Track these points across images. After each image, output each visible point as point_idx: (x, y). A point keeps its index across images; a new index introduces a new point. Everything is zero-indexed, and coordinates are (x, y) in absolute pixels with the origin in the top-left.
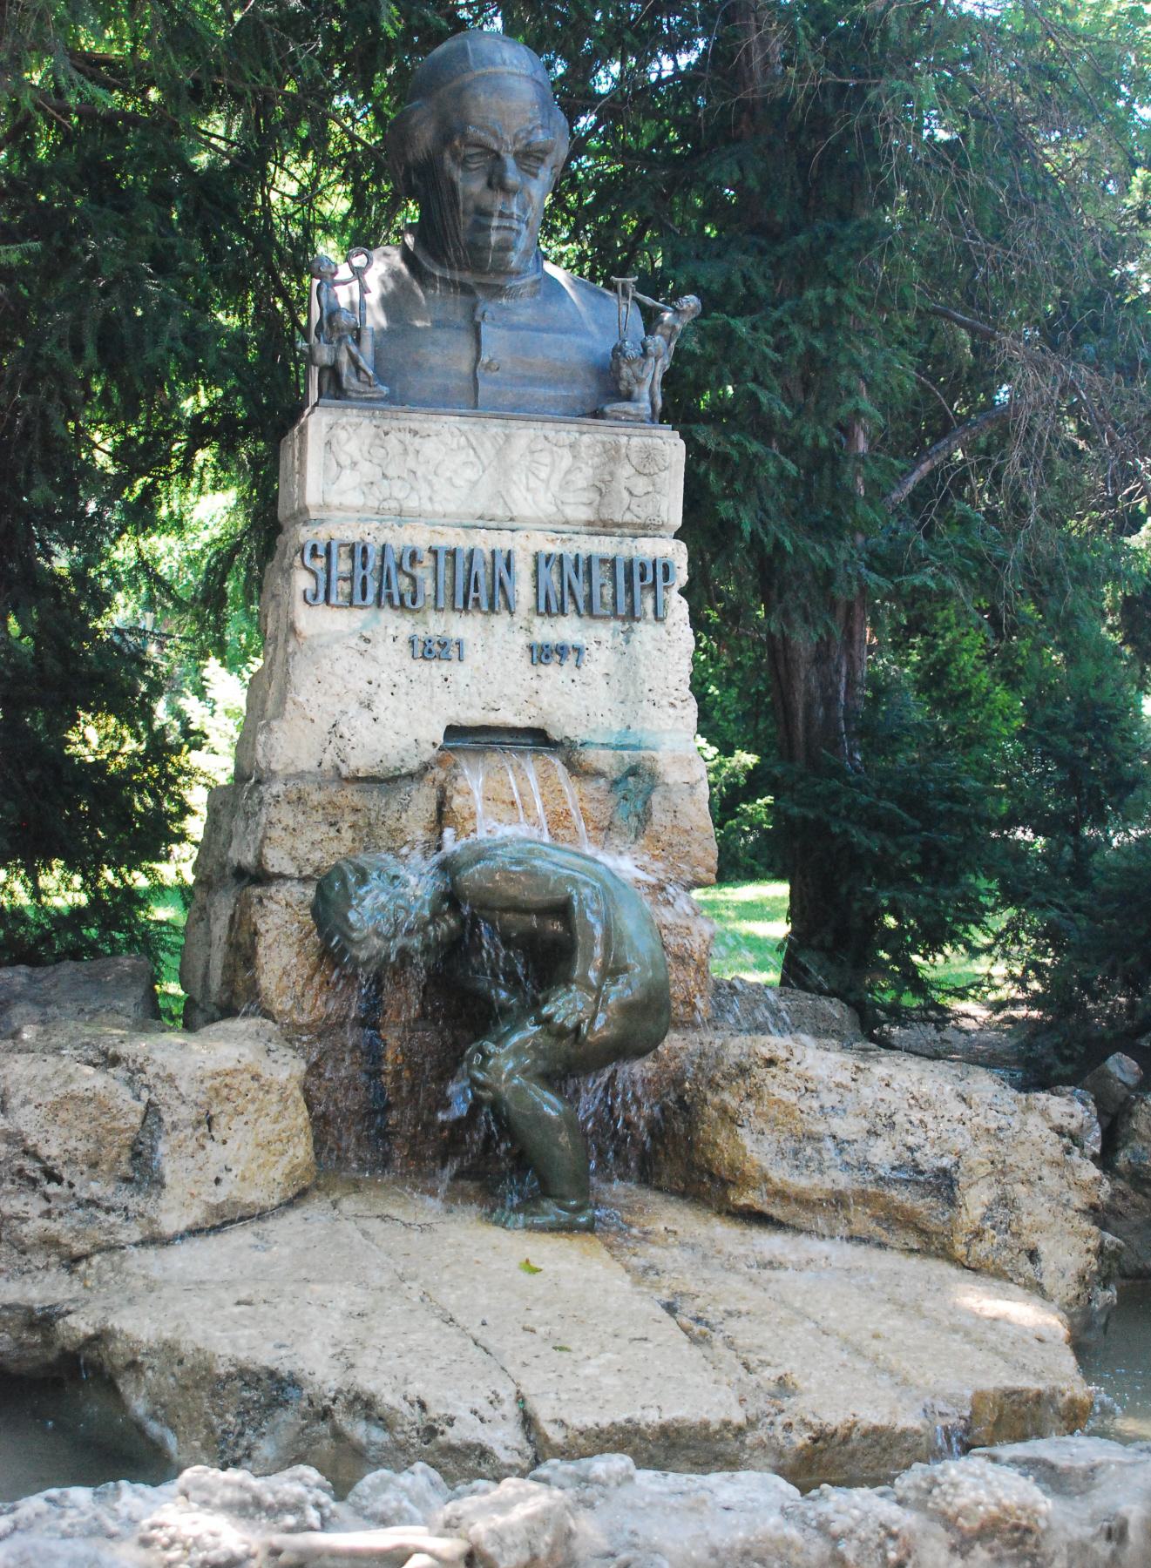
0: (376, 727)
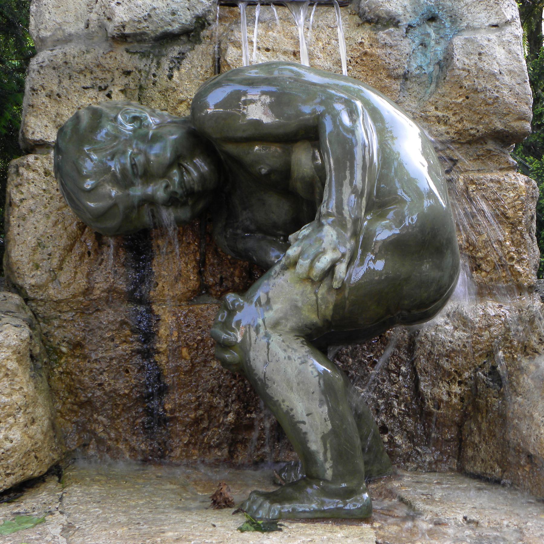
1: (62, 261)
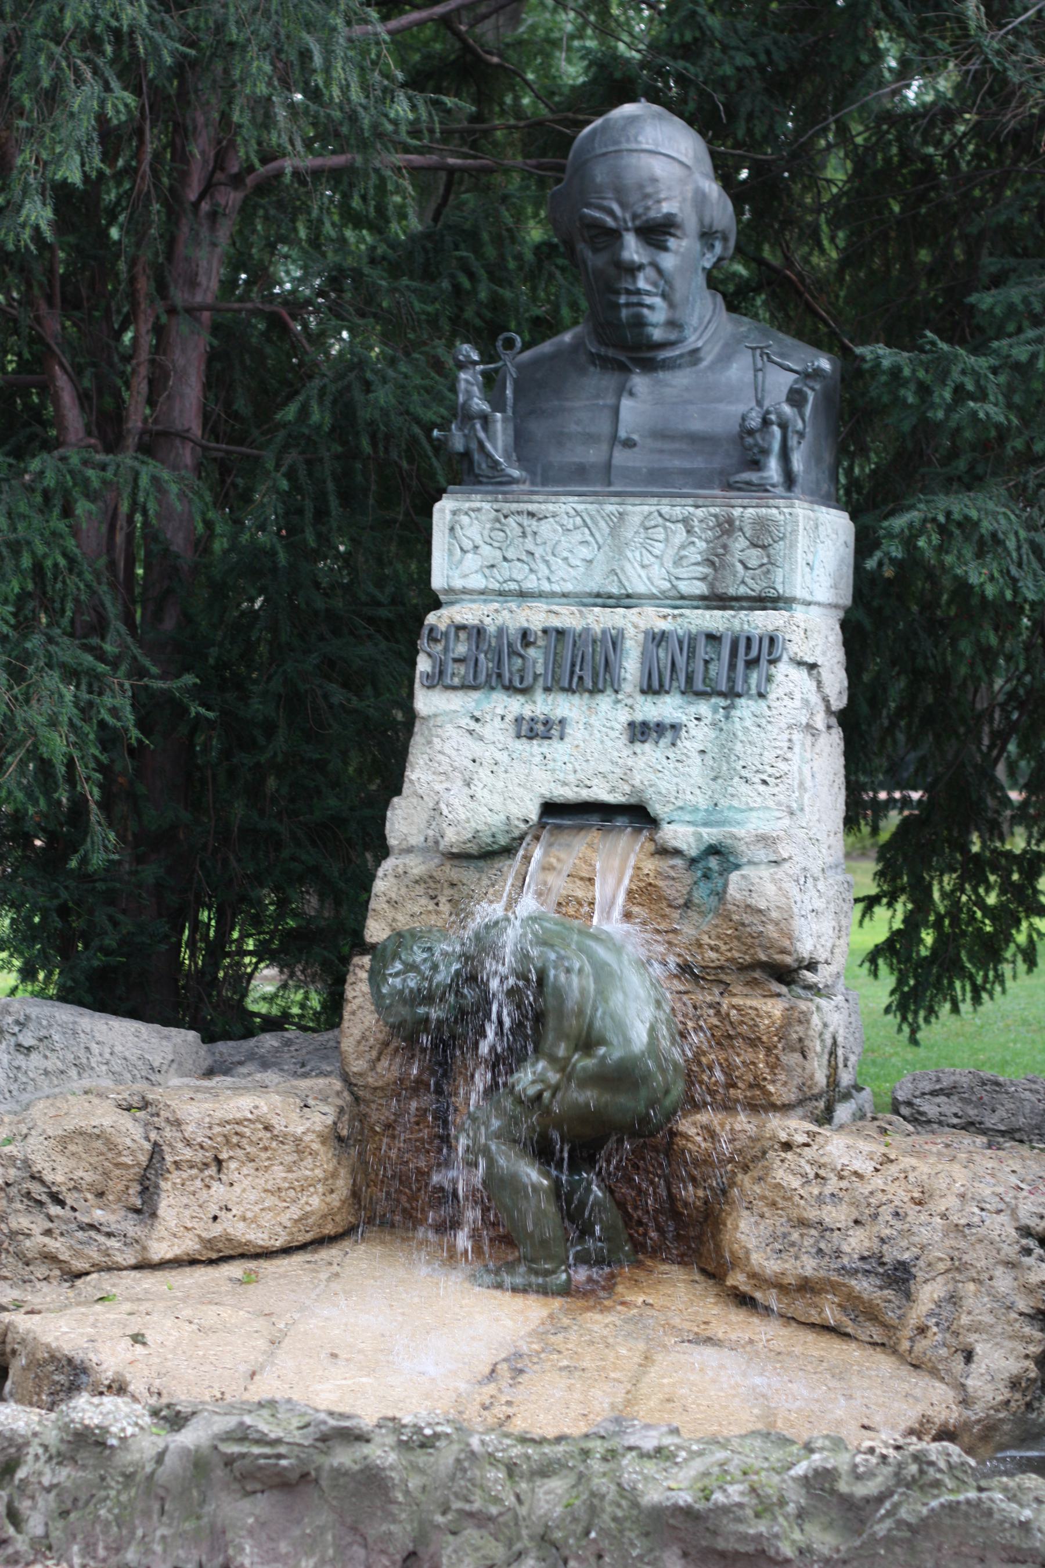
0: (473, 805)
1: (380, 1054)
